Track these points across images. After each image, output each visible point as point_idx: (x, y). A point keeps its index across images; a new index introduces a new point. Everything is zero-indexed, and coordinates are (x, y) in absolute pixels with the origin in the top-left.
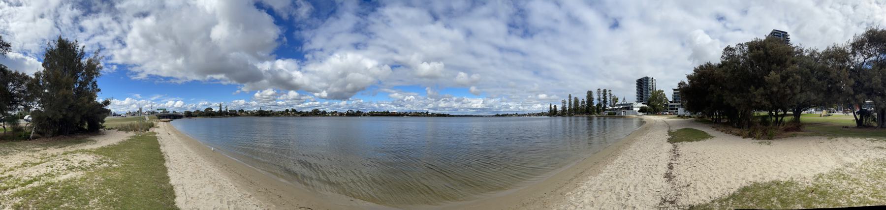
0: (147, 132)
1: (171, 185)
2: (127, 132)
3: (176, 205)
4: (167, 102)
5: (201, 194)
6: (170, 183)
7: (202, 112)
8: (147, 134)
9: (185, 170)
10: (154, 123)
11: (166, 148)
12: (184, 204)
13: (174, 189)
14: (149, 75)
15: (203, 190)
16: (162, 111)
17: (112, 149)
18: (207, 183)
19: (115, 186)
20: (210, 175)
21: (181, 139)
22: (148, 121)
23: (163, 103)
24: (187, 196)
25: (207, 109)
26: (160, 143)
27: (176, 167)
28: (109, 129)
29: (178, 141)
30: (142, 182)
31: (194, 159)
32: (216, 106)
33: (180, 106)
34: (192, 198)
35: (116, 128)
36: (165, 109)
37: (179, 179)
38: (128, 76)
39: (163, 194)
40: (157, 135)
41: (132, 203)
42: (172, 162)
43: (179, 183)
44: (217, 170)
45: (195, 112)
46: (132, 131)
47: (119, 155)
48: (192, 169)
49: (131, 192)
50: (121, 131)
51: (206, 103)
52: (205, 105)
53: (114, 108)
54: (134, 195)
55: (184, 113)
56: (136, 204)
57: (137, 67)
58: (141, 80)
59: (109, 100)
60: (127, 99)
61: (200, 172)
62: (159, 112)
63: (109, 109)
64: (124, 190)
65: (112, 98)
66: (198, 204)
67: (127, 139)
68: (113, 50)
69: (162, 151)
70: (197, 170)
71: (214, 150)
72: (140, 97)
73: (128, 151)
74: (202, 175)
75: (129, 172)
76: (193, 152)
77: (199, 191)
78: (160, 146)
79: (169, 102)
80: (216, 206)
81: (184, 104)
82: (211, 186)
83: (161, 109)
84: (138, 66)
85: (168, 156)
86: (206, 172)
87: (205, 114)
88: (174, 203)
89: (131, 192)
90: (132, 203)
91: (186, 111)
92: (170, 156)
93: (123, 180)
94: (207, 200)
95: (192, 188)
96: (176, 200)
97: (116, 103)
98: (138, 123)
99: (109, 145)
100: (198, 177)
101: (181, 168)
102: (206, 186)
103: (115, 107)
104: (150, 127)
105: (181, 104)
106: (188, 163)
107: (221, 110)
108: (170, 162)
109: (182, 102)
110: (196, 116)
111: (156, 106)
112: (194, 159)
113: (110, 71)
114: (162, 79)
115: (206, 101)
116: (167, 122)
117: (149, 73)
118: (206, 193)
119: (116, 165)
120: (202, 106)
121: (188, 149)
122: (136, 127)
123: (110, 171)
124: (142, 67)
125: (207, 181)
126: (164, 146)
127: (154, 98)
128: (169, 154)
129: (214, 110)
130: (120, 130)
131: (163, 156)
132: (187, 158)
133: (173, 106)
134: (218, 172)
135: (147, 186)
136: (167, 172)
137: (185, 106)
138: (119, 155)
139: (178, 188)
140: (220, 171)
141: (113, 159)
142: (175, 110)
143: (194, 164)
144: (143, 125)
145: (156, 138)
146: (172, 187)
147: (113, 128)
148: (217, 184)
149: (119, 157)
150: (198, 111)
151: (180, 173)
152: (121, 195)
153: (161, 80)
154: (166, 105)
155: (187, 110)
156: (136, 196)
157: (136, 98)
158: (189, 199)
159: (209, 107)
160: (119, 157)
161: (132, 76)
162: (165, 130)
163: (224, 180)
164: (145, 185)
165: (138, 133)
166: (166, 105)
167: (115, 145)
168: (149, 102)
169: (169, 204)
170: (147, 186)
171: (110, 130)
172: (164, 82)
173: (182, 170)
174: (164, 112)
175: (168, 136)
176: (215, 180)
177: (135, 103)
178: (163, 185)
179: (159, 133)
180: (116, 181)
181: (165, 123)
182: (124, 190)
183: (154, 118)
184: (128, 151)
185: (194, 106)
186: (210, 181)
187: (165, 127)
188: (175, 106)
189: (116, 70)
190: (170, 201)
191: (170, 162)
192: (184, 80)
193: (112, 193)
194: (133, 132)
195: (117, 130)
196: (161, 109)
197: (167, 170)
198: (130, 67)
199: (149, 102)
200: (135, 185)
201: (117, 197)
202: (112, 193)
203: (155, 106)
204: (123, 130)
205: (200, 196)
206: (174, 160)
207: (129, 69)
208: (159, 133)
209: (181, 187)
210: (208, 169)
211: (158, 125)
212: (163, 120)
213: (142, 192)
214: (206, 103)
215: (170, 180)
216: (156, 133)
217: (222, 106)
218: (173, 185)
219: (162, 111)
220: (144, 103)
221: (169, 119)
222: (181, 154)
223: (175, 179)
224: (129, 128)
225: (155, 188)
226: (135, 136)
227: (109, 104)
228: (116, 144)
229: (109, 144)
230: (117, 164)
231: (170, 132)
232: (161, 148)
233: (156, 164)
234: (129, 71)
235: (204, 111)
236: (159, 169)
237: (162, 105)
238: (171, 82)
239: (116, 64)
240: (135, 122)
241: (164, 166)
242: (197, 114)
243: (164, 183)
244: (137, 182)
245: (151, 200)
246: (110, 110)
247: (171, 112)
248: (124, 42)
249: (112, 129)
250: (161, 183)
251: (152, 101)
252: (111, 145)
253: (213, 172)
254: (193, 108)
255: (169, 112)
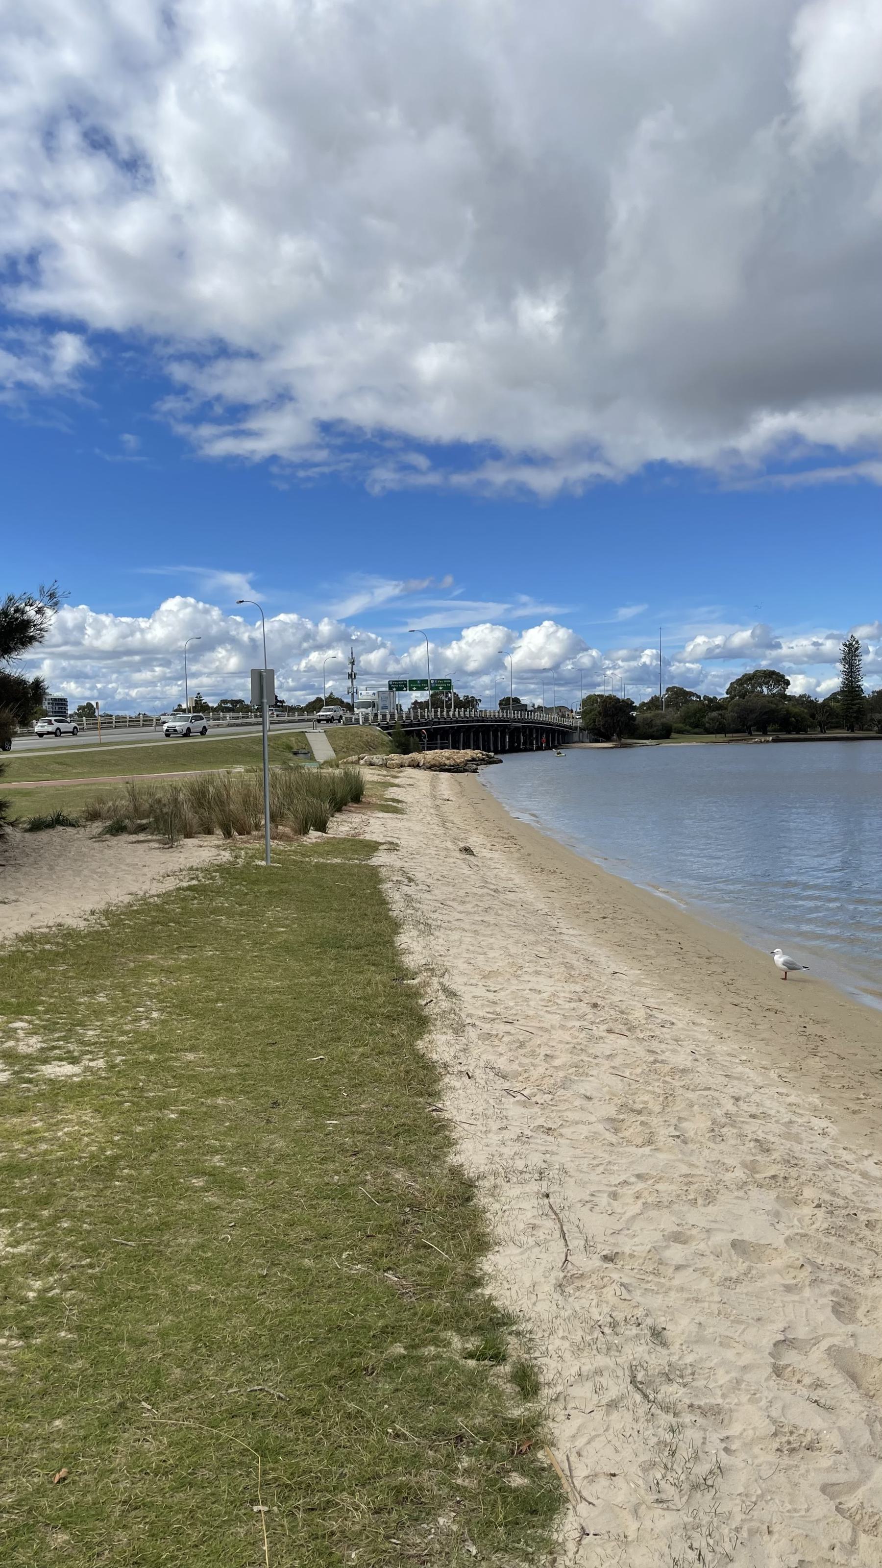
0: (314, 835)
1: (456, 1172)
2: (169, 844)
3: (487, 1291)
4: (456, 633)
5: (678, 1238)
6: (453, 1159)
7: (712, 704)
8: (315, 849)
9: (565, 1084)
10: (369, 775)
11: (438, 942)
12: (547, 1288)
13: (482, 1200)
14: (326, 427)
15: (696, 1217)
16: (423, 696)
17: (43, 960)
18: (728, 1176)
19: (45, 1201)
20: (753, 1128)
21: (555, 882)
22: (329, 763)
23: (427, 635)
24: (576, 1243)
25: (747, 679)
26: (397, 908)
27: (502, 1063)
28: (37, 826)
29: (530, 896)
30: (252, 1158)
31: (639, 1014)
32: (818, 658)
33: (545, 662)
34: (606, 1258)
35: (94, 816)
36: (447, 685)
37: (520, 1138)
38: (181, 429)
39: (395, 1230)
40: (381, 859)
41: (164, 1293)
42: (472, 1033)
43: (520, 1164)
44: (815, 1099)
45: (655, 703)
46: (209, 832)
47: (101, 998)
48: (615, 1082)
49: (160, 1228)
50: (125, 837)
51: (742, 637)
52: (729, 654)
53: (79, 676)
54: (188, 1240)
55: (577, 708)
56: (199, 1295)
57: (241, 366)
58: (274, 459)
59: (31, 612)
60: (172, 604)
61: (679, 1106)
62: (408, 699)
63: (30, 677)
64: (110, 1220)
65: (54, 600)
66: (656, 1302)
67: (170, 884)
68: (47, 204)
69: (410, 961)
70: (657, 1087)
71: (791, 966)
72: (252, 596)
73: (169, 971)
74: (695, 1126)
75: (163, 1105)
76: (632, 972)
77: (667, 1222)
78: (396, 926)
79: (470, 634)
80: (801, 1332)
81: (577, 647)
82: (767, 1199)
83: (419, 685)
84: (251, 355)
85: (451, 994)
86: (729, 1106)
87: (729, 714)
88: (477, 1283)
89: (160, 1228)
90: (164, 1293)
91: (590, 701)
92: (467, 993)
93: (116, 1158)
94: (728, 1282)
95: (614, 1196)
96: (487, 1264)
97: (89, 638)
98: (252, 779)
99: (29, 938)
100: (663, 1134)
101: (536, 1073)
102: (725, 1197)
103: (88, 666)
104: (339, 806)
105: (555, 648)
106: (591, 1038)
107: (851, 689)
108: (459, 1029)
109: (563, 633)
110: (665, 733)
111: (384, 663)
112: (639, 1014)
113: (35, 377)
114: (422, 461)
115: (734, 620)
116: (455, 769)
117: (326, 415)
118: (721, 1239)
119: (67, 1069)
120: (711, 656)
121: (601, 955)
122: (235, 806)
123: (21, 1111)
124: (271, 367)
125: (730, 1161)
126: (427, 928)
127: (354, 605)
128: (456, 983)
129: (797, 687)
130: (117, 829)
131: (414, 994)
132: (584, 1008)
133: (496, 663)
134: (815, 1111)
135: (283, 1183)
136: (436, 1095)
137: (585, 659)
138: (101, 998)
139: (512, 1191)
140: (835, 1110)
141: (49, 1028)
142: (512, 689)
143: (640, 1050)
144: (289, 793)
145: (374, 876)
146: (470, 1185)
147: (72, 812)
148: (809, 1193)
149: (98, 1012)
150: (679, 696)
151: (527, 1102)
152: (89, 1250)
153: (406, 468)
154: (452, 652)
155: (598, 691)
156: (202, 1247)
157: (217, 598)
158: (582, 1262)
159: (764, 664)
160: (98, 1012)
161: (206, 430)
162: (444, 823)
163: (864, 1175)
164: (271, 1175)
165: (250, 844)
166: (452, 652)
167: (70, 934)
168: (325, 628)
169: (438, 1286)
170: (283, 1183)
171: (44, 836)
172: (433, 479)
173: (547, 1083)
174: (435, 702)
175: (461, 867)
176: (791, 1161)
177: (226, 639)
178: (399, 1175)
179: (393, 847)
180: (60, 1173)
181: (445, 775)
182: (110, 1220)
183: (370, 747)
184: (169, 971)
185: (647, 657)
186: (752, 1168)
187: (438, 803)
188: (515, 659)
189: (81, 372)
190: (442, 1271)
191: (459, 1029)
192: (583, 470)
193: (22, 1249)
194: (217, 838)
195: (97, 827)
196: (419, 685)
197: (438, 1079)
198: (180, 358)
199: (325, 628)
200: (198, 1182)
201: (54, 1266)
202: (22, 1249)
203: (373, 658)
204: (142, 829)
205: (676, 1253)
206: (496, 1017)
207: (179, 372)
208: (393, 847)
209: (533, 1187)
210: (737, 1088)
211: (392, 793)
212: (430, 755)
213: (241, 1223)
214: (742, 637)
215: (450, 1143)
216: (372, 847)
217: (867, 660)
218: (470, 1172)
219: (423, 696)
220: (291, 637)
221: (469, 753)
222: (546, 985)
223: (494, 1138)
224: (188, 813)
225: (343, 1193)
226: (222, 869)
227: (26, 641)
228: (82, 924)
229: (22, 929)
230: (74, 1061)
231: (474, 840)
232: (406, 939)
233: (360, 1042)
234: (183, 390)
235: (721, 694)
236: (377, 1078)
237: (420, 652)
238: (483, 484)
239: (77, 327)
240: (239, 769)
241: (419, 1057)
242: (671, 716)
243: (406, 1162)
244: (217, 1161)
245: (307, 1262)
246: (37, 685)
247: (489, 707)
248: (130, 140)
249: (59, 821)
250: (387, 1159)
251: (350, 621)
252: (46, 939)
253: (771, 1106)
254: (641, 676)
255: (470, 703)
